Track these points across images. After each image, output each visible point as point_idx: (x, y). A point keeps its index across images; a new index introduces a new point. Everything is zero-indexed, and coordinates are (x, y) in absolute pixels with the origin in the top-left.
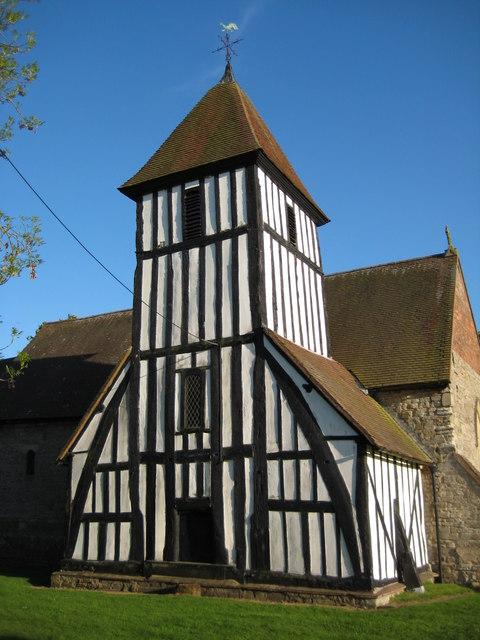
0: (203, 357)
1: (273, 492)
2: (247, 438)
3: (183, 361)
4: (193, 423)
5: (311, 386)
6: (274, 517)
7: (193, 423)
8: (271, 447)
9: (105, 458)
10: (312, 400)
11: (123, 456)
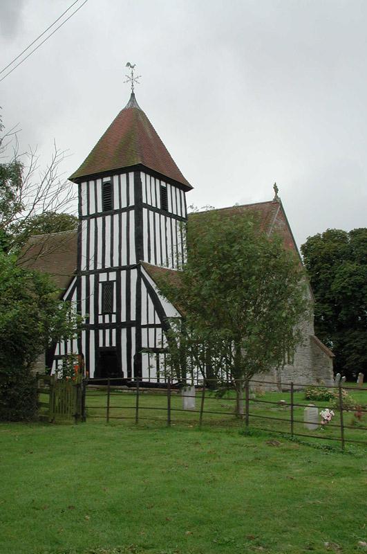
0: (113, 276)
1: (144, 345)
2: (133, 318)
4: (107, 310)
6: (145, 356)
7: (107, 310)
8: (144, 322)
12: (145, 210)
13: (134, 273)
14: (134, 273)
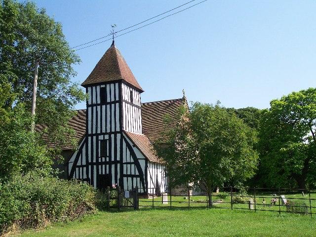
0: (107, 137)
1: (125, 173)
3: (101, 138)
4: (104, 154)
5: (135, 145)
8: (124, 161)
9: (79, 164)
10: (135, 149)
11: (84, 163)
12: (124, 103)
13: (119, 136)
14: (119, 136)
